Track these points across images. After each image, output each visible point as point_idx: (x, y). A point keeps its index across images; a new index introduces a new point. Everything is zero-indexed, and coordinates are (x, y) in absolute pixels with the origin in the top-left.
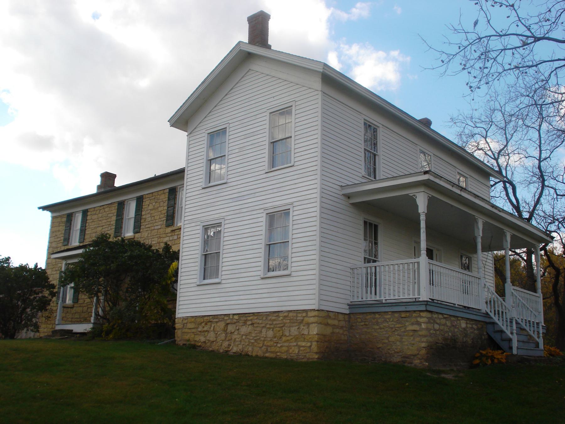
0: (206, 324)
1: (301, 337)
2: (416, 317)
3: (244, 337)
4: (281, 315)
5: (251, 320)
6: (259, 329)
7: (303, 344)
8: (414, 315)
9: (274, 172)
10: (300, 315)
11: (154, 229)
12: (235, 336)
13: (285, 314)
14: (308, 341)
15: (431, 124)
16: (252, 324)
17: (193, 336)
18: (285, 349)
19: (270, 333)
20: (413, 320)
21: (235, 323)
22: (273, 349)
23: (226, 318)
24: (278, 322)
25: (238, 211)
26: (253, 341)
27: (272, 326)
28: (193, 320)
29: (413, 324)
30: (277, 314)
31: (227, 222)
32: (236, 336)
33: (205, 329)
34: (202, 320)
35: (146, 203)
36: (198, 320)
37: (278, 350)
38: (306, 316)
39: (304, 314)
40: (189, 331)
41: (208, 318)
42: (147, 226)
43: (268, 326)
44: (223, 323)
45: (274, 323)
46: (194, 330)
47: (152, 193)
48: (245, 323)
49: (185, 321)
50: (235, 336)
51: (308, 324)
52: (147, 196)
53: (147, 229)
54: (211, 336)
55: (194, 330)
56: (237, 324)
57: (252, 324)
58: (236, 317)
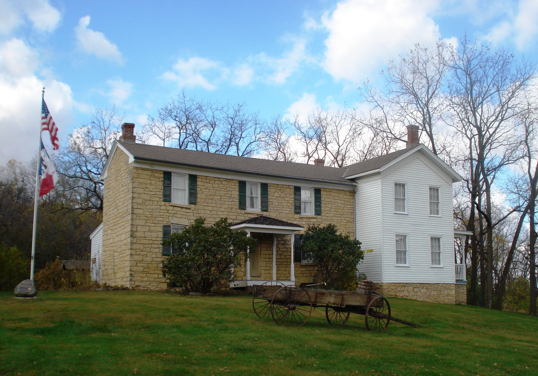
0: (401, 287)
1: (448, 295)
2: (463, 287)
3: (424, 294)
4: (440, 285)
5: (426, 286)
6: (430, 291)
7: (450, 298)
8: (463, 286)
9: (234, 169)
10: (448, 286)
11: (282, 213)
12: (419, 294)
13: (442, 285)
14: (452, 297)
15: (126, 123)
16: (427, 288)
17: (395, 293)
18: (443, 300)
19: (435, 293)
20: (462, 288)
21: (418, 288)
22: (437, 300)
23: (413, 285)
24: (438, 288)
25: (415, 232)
26: (428, 296)
27: (436, 290)
28: (394, 285)
29: (462, 290)
30: (438, 285)
31: (410, 236)
32: (419, 294)
33: (402, 290)
34: (399, 285)
35: (271, 190)
36: (398, 285)
37: (439, 300)
38: (450, 286)
39: (450, 285)
40: (392, 290)
41: (403, 284)
42: (275, 208)
43: (434, 290)
44: (412, 287)
45: (437, 288)
46: (395, 290)
47: (278, 185)
48: (423, 288)
49: (390, 285)
50: (419, 294)
51: (451, 289)
52: (271, 185)
53: (275, 211)
54: (406, 293)
55: (395, 290)
56: (419, 288)
57: (427, 288)
58: (419, 284)
